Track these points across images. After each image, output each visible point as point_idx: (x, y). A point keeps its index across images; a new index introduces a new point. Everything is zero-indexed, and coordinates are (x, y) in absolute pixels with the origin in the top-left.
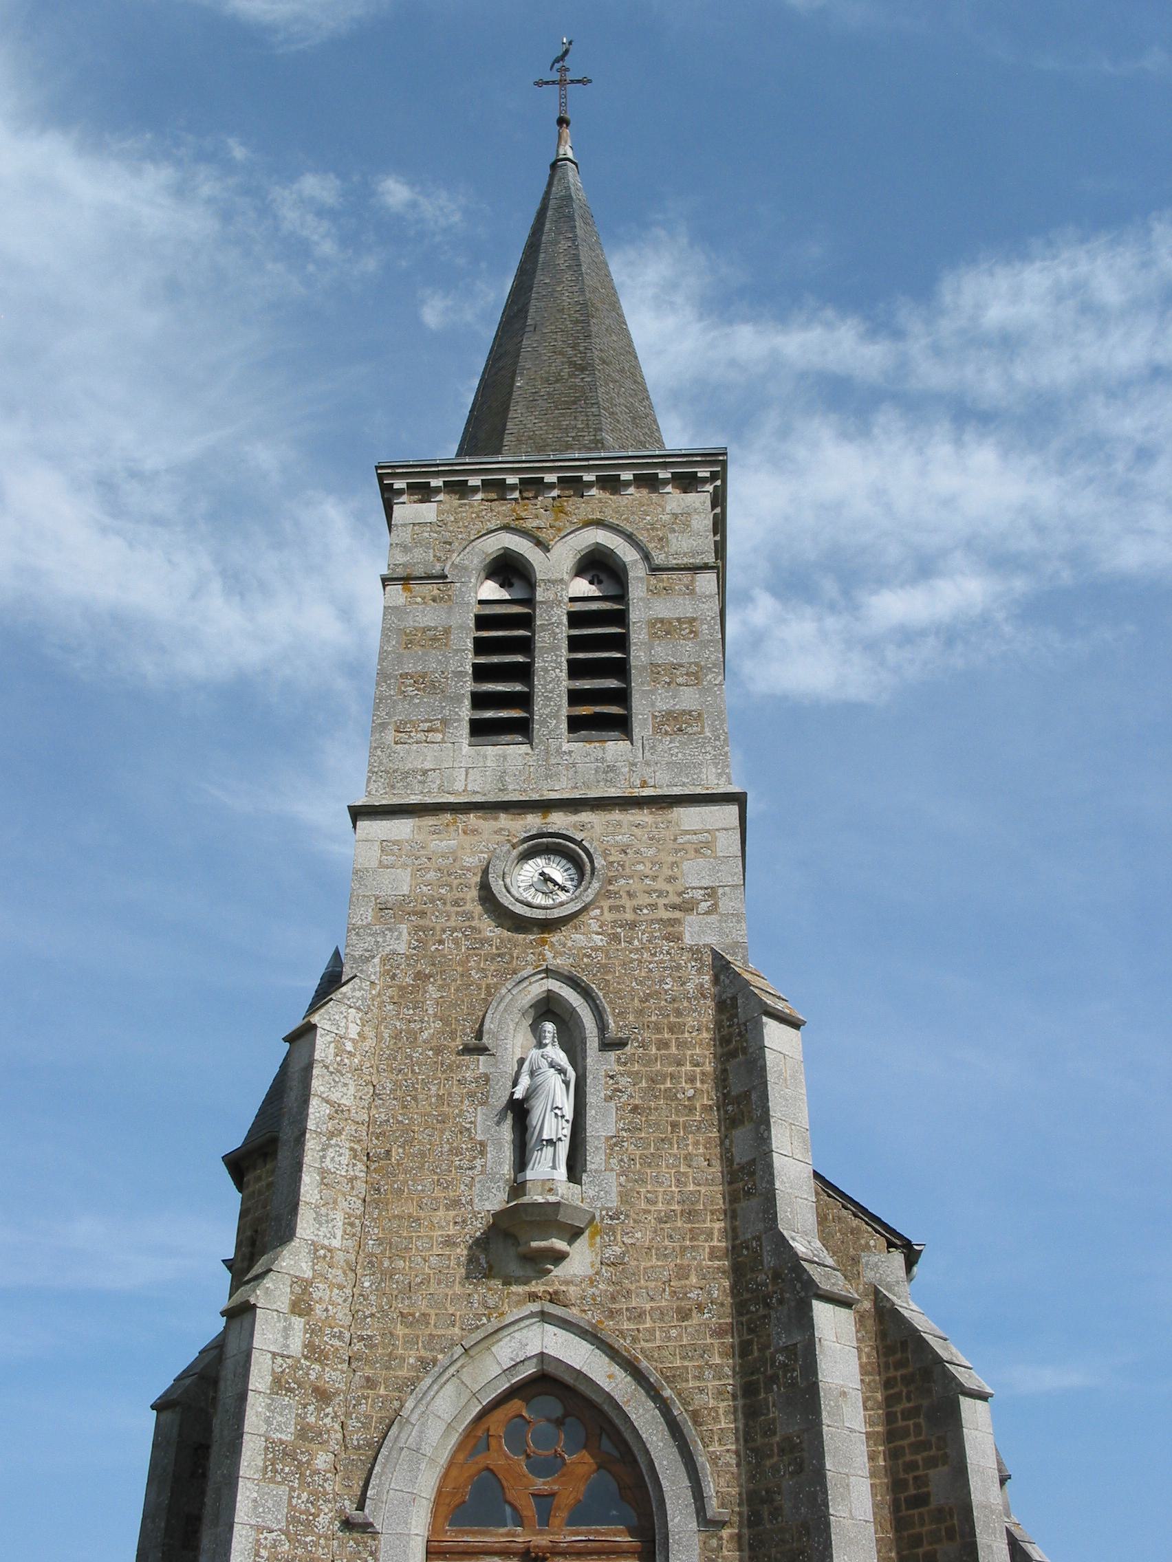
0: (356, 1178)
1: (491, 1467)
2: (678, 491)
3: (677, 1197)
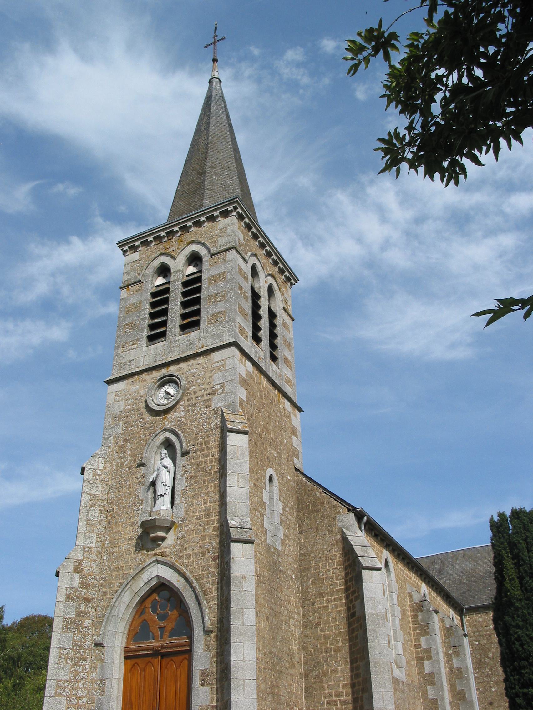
0: (102, 520)
1: (146, 619)
2: (223, 218)
3: (204, 509)
